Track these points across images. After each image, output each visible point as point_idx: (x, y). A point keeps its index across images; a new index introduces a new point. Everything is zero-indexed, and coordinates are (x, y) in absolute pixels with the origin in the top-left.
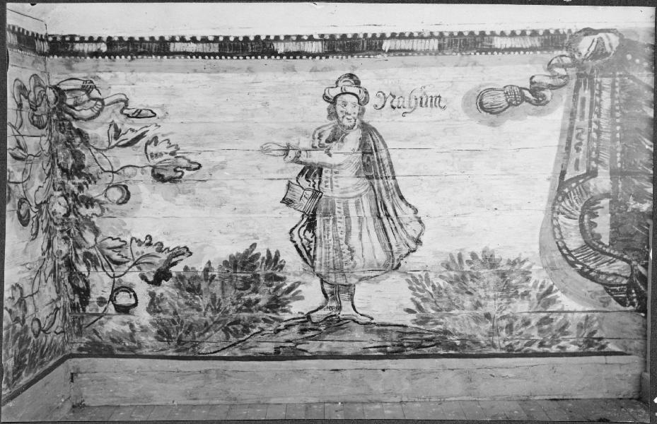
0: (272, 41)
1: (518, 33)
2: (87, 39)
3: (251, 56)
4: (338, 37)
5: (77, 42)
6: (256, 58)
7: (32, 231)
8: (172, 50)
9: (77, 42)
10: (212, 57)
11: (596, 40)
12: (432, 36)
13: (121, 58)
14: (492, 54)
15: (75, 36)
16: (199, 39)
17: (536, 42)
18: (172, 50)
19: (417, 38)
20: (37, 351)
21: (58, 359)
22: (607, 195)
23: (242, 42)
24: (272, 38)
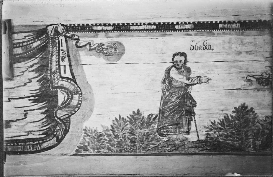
0: (218, 23)
1: (180, 23)
2: (223, 22)
3: (247, 30)
4: (170, 23)
5: (94, 26)
6: (122, 32)
7: (65, 81)
8: (131, 29)
9: (94, 26)
10: (190, 31)
11: (54, 28)
12: (109, 25)
13: (227, 30)
14: (176, 31)
15: (205, 22)
16: (227, 22)
17: (111, 28)
18: (220, 27)
19: (223, 23)
20: (112, 146)
21: (181, 176)
22: (79, 95)
23: (77, 27)
24: (218, 22)
